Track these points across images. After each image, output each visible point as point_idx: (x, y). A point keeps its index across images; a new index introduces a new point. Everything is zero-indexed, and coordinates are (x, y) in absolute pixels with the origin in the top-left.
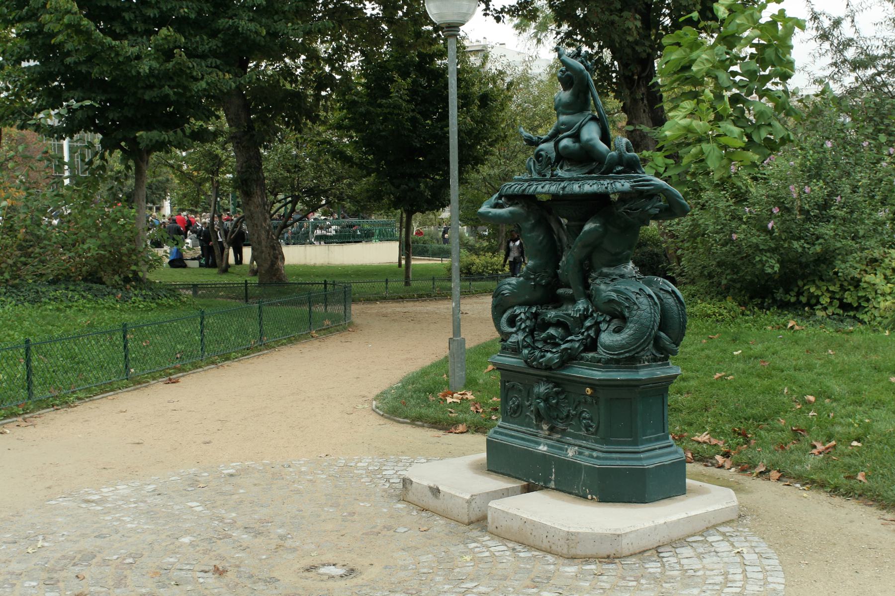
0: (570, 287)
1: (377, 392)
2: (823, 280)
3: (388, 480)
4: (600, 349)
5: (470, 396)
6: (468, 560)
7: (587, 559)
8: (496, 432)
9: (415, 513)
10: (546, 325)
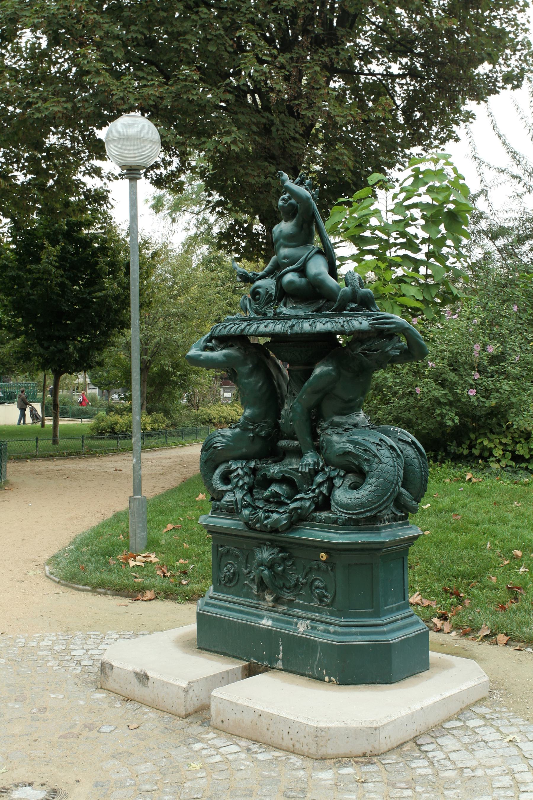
0: (296, 439)
1: (48, 555)
2: (494, 433)
3: (79, 663)
4: (335, 508)
5: (153, 558)
6: (198, 768)
7: (341, 760)
8: (207, 604)
9: (118, 705)
10: (267, 482)
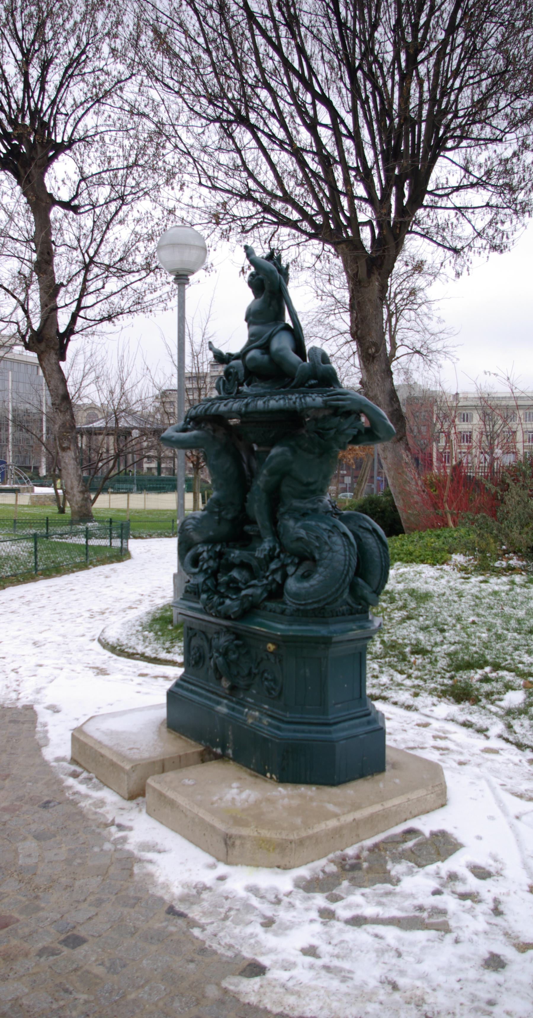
4: (287, 598)
10: (231, 566)
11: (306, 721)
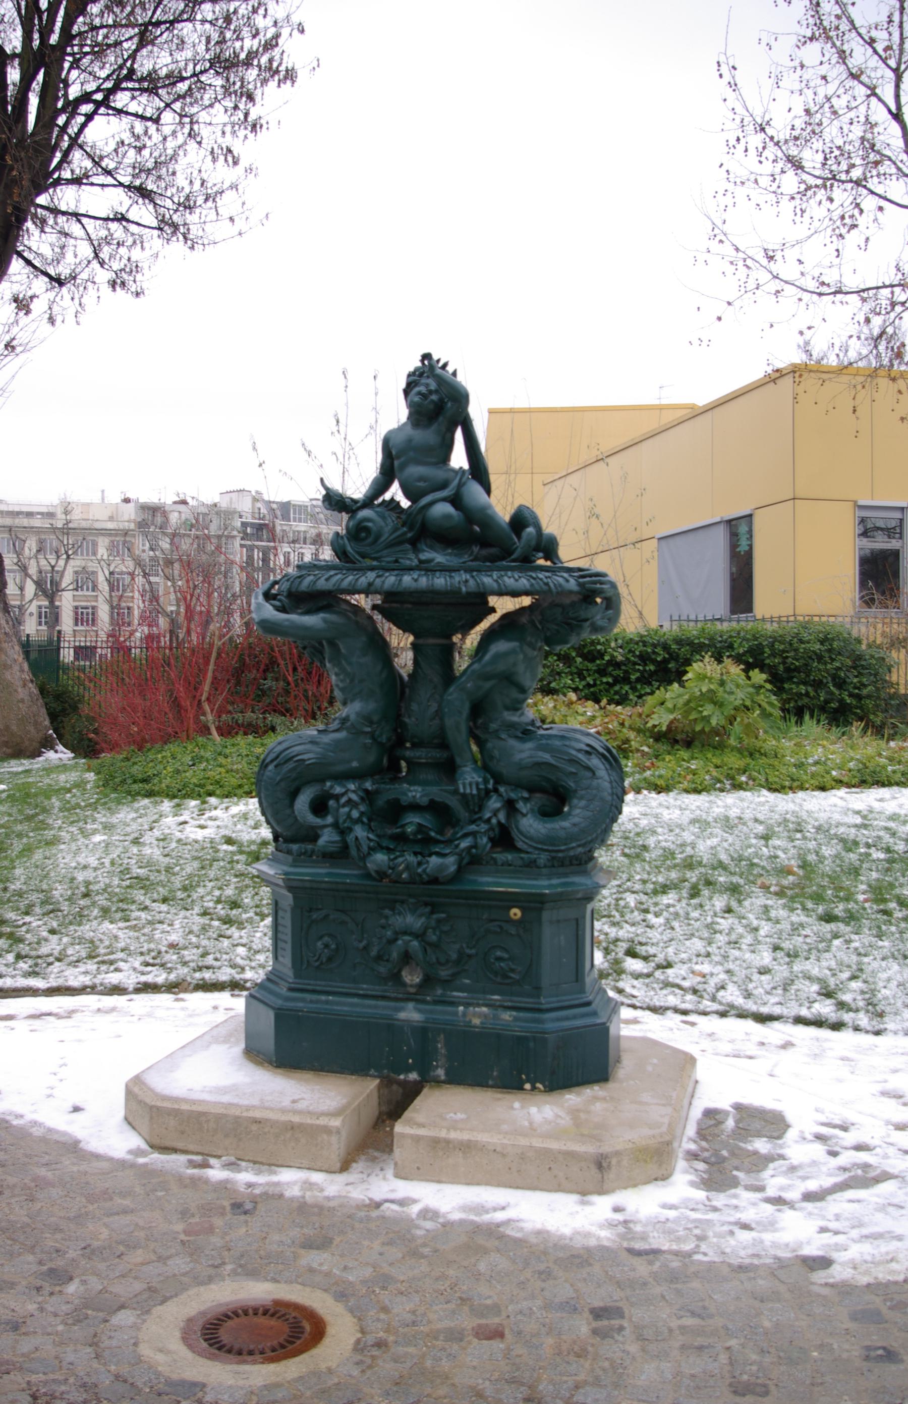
11: (566, 1003)
